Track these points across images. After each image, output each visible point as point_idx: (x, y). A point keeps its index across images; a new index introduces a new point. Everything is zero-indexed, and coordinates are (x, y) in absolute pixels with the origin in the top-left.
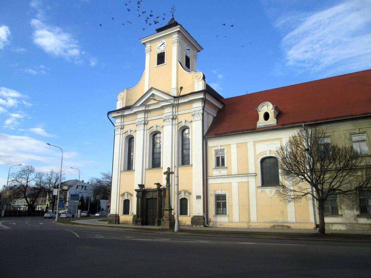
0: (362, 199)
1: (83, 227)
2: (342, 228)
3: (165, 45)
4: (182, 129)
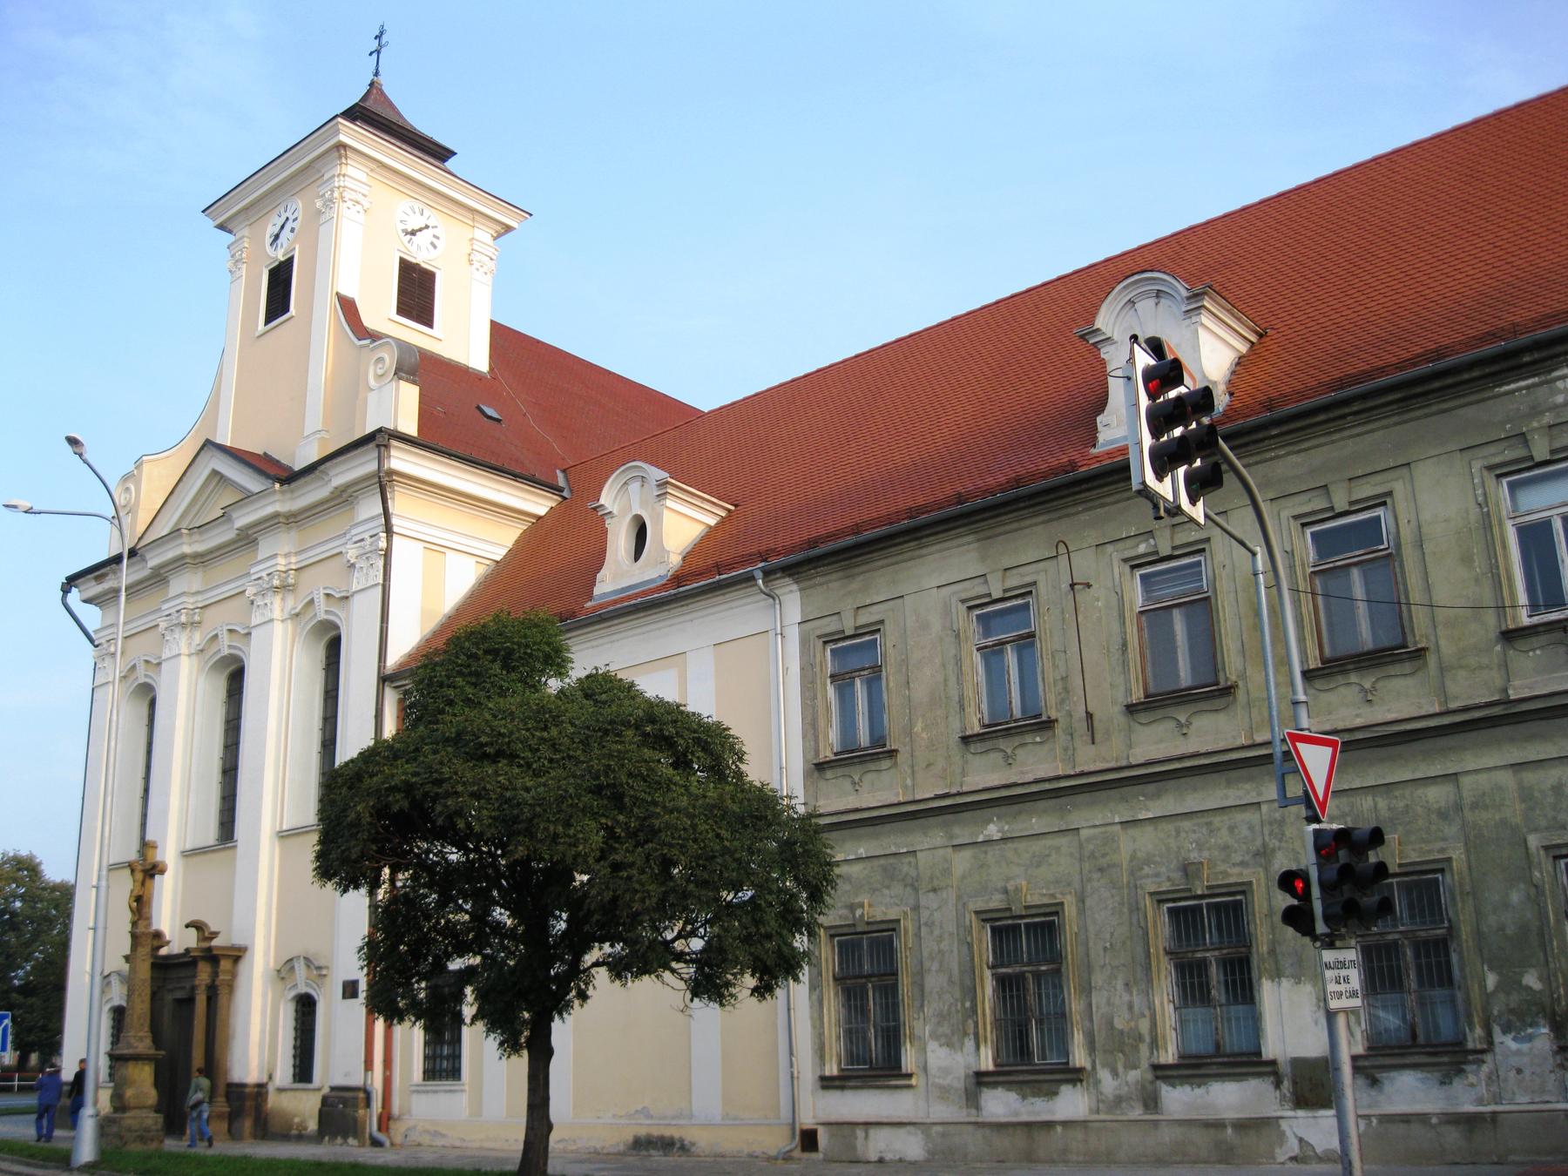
0: (1009, 976)
3: (296, 225)
4: (228, 666)
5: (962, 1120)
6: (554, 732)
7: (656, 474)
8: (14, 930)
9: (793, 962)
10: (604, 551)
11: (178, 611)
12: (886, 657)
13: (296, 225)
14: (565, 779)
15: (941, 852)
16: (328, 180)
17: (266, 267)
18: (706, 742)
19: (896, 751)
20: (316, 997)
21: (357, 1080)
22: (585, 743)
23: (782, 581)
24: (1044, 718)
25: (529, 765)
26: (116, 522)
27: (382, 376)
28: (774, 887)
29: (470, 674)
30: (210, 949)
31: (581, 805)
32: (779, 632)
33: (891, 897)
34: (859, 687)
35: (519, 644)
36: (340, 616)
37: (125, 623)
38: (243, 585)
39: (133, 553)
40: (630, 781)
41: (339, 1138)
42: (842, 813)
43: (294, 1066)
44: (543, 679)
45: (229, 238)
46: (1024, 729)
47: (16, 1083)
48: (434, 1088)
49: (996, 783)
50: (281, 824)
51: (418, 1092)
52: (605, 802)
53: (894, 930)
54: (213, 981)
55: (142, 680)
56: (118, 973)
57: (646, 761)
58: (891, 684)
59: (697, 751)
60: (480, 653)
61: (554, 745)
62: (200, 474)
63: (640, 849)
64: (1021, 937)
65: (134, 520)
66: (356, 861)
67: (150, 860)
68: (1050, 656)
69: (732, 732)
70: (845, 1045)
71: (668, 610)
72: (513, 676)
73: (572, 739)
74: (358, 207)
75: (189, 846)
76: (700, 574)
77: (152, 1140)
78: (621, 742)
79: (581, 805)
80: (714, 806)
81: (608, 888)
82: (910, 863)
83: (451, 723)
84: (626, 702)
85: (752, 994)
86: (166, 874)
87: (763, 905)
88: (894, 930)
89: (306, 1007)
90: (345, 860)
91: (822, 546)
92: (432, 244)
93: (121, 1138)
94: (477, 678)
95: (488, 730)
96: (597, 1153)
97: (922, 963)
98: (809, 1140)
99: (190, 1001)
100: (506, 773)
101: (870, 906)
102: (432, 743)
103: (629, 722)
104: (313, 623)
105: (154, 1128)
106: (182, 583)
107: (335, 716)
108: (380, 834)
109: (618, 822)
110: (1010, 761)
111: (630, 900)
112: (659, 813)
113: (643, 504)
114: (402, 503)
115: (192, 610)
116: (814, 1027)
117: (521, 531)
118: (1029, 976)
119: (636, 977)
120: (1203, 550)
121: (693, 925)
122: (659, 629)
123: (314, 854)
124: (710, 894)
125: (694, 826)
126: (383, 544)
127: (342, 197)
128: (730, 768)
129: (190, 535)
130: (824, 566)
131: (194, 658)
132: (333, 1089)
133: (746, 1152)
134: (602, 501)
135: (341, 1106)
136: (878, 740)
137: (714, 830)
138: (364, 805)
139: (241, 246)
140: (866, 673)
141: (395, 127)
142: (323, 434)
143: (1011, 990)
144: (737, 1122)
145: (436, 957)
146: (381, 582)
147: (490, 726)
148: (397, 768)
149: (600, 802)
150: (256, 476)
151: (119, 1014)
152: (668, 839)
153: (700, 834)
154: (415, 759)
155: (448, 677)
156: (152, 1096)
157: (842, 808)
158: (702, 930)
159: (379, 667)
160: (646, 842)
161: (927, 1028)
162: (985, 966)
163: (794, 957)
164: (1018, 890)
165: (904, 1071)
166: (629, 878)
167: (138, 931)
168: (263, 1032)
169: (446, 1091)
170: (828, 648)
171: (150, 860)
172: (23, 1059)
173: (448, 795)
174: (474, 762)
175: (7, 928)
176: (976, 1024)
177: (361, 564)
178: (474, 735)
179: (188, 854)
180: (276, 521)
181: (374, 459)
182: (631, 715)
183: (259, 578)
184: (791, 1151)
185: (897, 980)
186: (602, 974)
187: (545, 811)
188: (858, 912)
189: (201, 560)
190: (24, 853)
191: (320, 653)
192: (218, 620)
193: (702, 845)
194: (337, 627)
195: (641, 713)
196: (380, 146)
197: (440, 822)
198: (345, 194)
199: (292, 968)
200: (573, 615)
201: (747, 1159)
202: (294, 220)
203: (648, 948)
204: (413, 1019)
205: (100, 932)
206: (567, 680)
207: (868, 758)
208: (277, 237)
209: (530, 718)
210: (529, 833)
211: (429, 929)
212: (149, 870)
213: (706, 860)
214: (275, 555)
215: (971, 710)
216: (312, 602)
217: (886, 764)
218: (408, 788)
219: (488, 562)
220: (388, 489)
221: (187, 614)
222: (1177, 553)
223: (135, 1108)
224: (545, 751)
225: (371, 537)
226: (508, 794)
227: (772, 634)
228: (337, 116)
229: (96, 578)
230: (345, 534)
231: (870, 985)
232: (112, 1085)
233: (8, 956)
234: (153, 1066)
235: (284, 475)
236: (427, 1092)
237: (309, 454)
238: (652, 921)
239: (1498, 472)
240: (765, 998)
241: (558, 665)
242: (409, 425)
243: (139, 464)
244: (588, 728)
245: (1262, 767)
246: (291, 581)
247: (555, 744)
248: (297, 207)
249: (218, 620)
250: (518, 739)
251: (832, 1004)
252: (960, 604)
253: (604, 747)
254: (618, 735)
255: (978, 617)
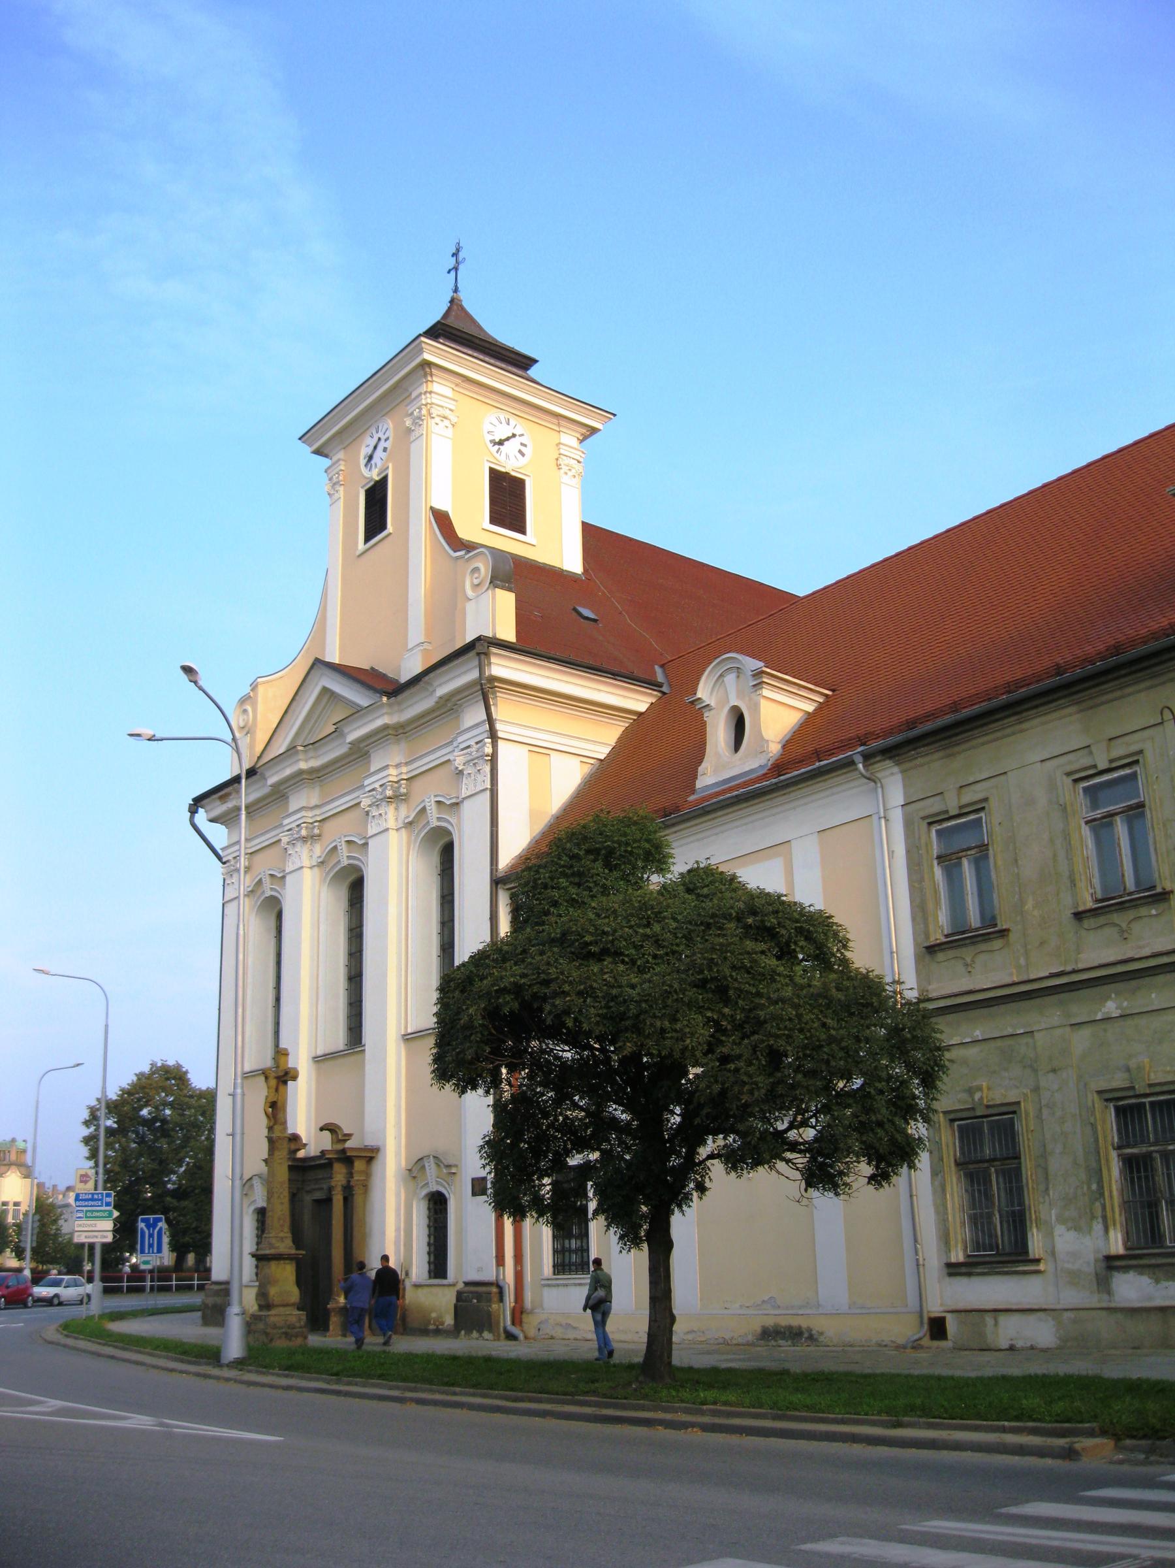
1: (994, 1195)
2: (1042, 1333)
3: (388, 444)
5: (1093, 1306)
6: (657, 928)
7: (755, 664)
8: (165, 1137)
9: (908, 1149)
10: (704, 744)
11: (298, 826)
12: (992, 836)
13: (388, 444)
14: (669, 974)
15: (1058, 1032)
16: (415, 399)
17: (362, 487)
18: (809, 931)
19: (1007, 930)
20: (447, 1195)
21: (489, 1274)
22: (688, 938)
23: (883, 763)
24: (1159, 890)
25: (633, 962)
26: (233, 745)
27: (478, 585)
28: (884, 1075)
29: (573, 875)
30: (344, 1151)
31: (686, 1000)
32: (882, 815)
33: (1010, 1079)
34: (967, 867)
35: (619, 843)
36: (451, 821)
37: (247, 840)
38: (358, 797)
39: (251, 773)
40: (734, 974)
41: (475, 1332)
42: (956, 995)
43: (429, 1263)
44: (645, 876)
45: (326, 462)
46: (1139, 902)
47: (174, 1283)
48: (565, 1282)
49: (1112, 959)
50: (406, 1027)
51: (549, 1285)
52: (710, 995)
53: (1014, 1112)
54: (349, 1182)
55: (269, 893)
56: (259, 1176)
57: (748, 953)
58: (999, 863)
59: (800, 941)
60: (582, 853)
61: (657, 942)
62: (312, 692)
63: (746, 1041)
64: (1146, 1116)
65: (253, 741)
66: (471, 1063)
67: (282, 1067)
68: (1161, 826)
69: (835, 920)
70: (971, 1230)
71: (824, 781)
72: (616, 874)
73: (675, 934)
74: (446, 422)
75: (319, 1053)
76: (801, 762)
77: (296, 1336)
78: (724, 935)
79: (686, 1000)
80: (819, 995)
81: (716, 1081)
82: (1027, 1043)
83: (554, 925)
84: (728, 895)
85: (869, 1183)
86: (299, 1078)
87: (873, 1091)
88: (1014, 1112)
89: (438, 1204)
90: (460, 1063)
91: (921, 726)
92: (520, 452)
93: (267, 1334)
94: (580, 878)
95: (592, 929)
96: (725, 1343)
97: (1044, 1146)
98: (937, 1328)
99: (328, 1201)
100: (612, 971)
101: (989, 1089)
102: (538, 944)
103: (731, 915)
104: (426, 831)
105: (298, 1325)
106: (302, 798)
107: (452, 920)
108: (493, 1035)
109: (724, 1015)
110: (1126, 935)
111: (739, 1093)
112: (764, 1005)
113: (740, 694)
114: (505, 710)
115: (312, 823)
116: (937, 1212)
117: (623, 728)
118: (1157, 1156)
119: (752, 1169)
120: (983, 809)
121: (803, 1115)
122: (763, 819)
123: (432, 1057)
124: (818, 1083)
125: (799, 1016)
126: (488, 750)
127: (430, 414)
128: (836, 957)
129: (305, 752)
130: (924, 746)
131: (316, 870)
132: (467, 1284)
133: (874, 1341)
134: (699, 695)
135: (475, 1301)
136: (989, 920)
137: (819, 1019)
138: (475, 1007)
139: (337, 470)
140: (973, 852)
141: (477, 341)
142: (426, 646)
143: (1139, 1171)
144: (864, 1311)
145: (556, 1153)
146: (489, 787)
147: (593, 925)
148: (506, 971)
149: (705, 995)
150: (363, 690)
151: (261, 1213)
152: (774, 1031)
153: (806, 1024)
154: (523, 961)
155: (552, 878)
156: (294, 1294)
157: (956, 990)
158: (813, 1120)
159: (492, 870)
160: (754, 1033)
161: (1053, 1212)
162: (1110, 1148)
163: (909, 1144)
164: (1140, 1068)
165: (1031, 1256)
166: (737, 1070)
167: (274, 1135)
168: (398, 1230)
169: (575, 1285)
170: (934, 829)
171: (282, 1067)
172: (180, 1260)
173: (555, 994)
174: (580, 961)
175: (159, 1135)
176: (1104, 1207)
177: (469, 770)
178: (579, 935)
179: (319, 1060)
180: (386, 733)
181: (475, 667)
182: (732, 908)
183: (373, 790)
184: (920, 1339)
185: (1020, 1163)
186: (717, 1168)
187: (651, 1006)
188: (977, 1096)
189: (316, 776)
190: (171, 1062)
191: (435, 859)
192: (336, 833)
193: (808, 1034)
194: (449, 833)
195: (741, 905)
196: (463, 361)
197: (549, 1022)
198: (432, 411)
199: (423, 1167)
200: (677, 809)
201: (875, 1348)
202: (386, 440)
203: (759, 1139)
204: (535, 1215)
205: (238, 1137)
206: (669, 876)
207: (980, 939)
208: (371, 458)
209: (632, 915)
210: (637, 1029)
211: (549, 1126)
212: (281, 1077)
213: (813, 1049)
214: (387, 767)
215: (1082, 884)
216: (424, 809)
217: (997, 944)
218: (517, 990)
219: (592, 761)
220: (491, 696)
221: (306, 828)
222: (1114, 765)
223: (277, 1306)
224: (649, 948)
225: (477, 743)
226: (614, 992)
227: (875, 818)
228: (420, 335)
229: (221, 798)
230: (452, 741)
231: (993, 1169)
232: (257, 1284)
233: (161, 1162)
234: (294, 1265)
235: (390, 688)
236: (558, 1285)
237: (412, 666)
238: (763, 1111)
239: (930, 820)
240: (882, 1186)
241: (659, 861)
242: (507, 632)
243: (254, 687)
244: (690, 923)
245: (1052, 997)
246: (403, 791)
247: (658, 940)
248: (388, 427)
249: (336, 833)
250: (621, 937)
251: (955, 1189)
252: (1065, 777)
253: (707, 940)
254: (720, 928)
255: (1085, 790)
